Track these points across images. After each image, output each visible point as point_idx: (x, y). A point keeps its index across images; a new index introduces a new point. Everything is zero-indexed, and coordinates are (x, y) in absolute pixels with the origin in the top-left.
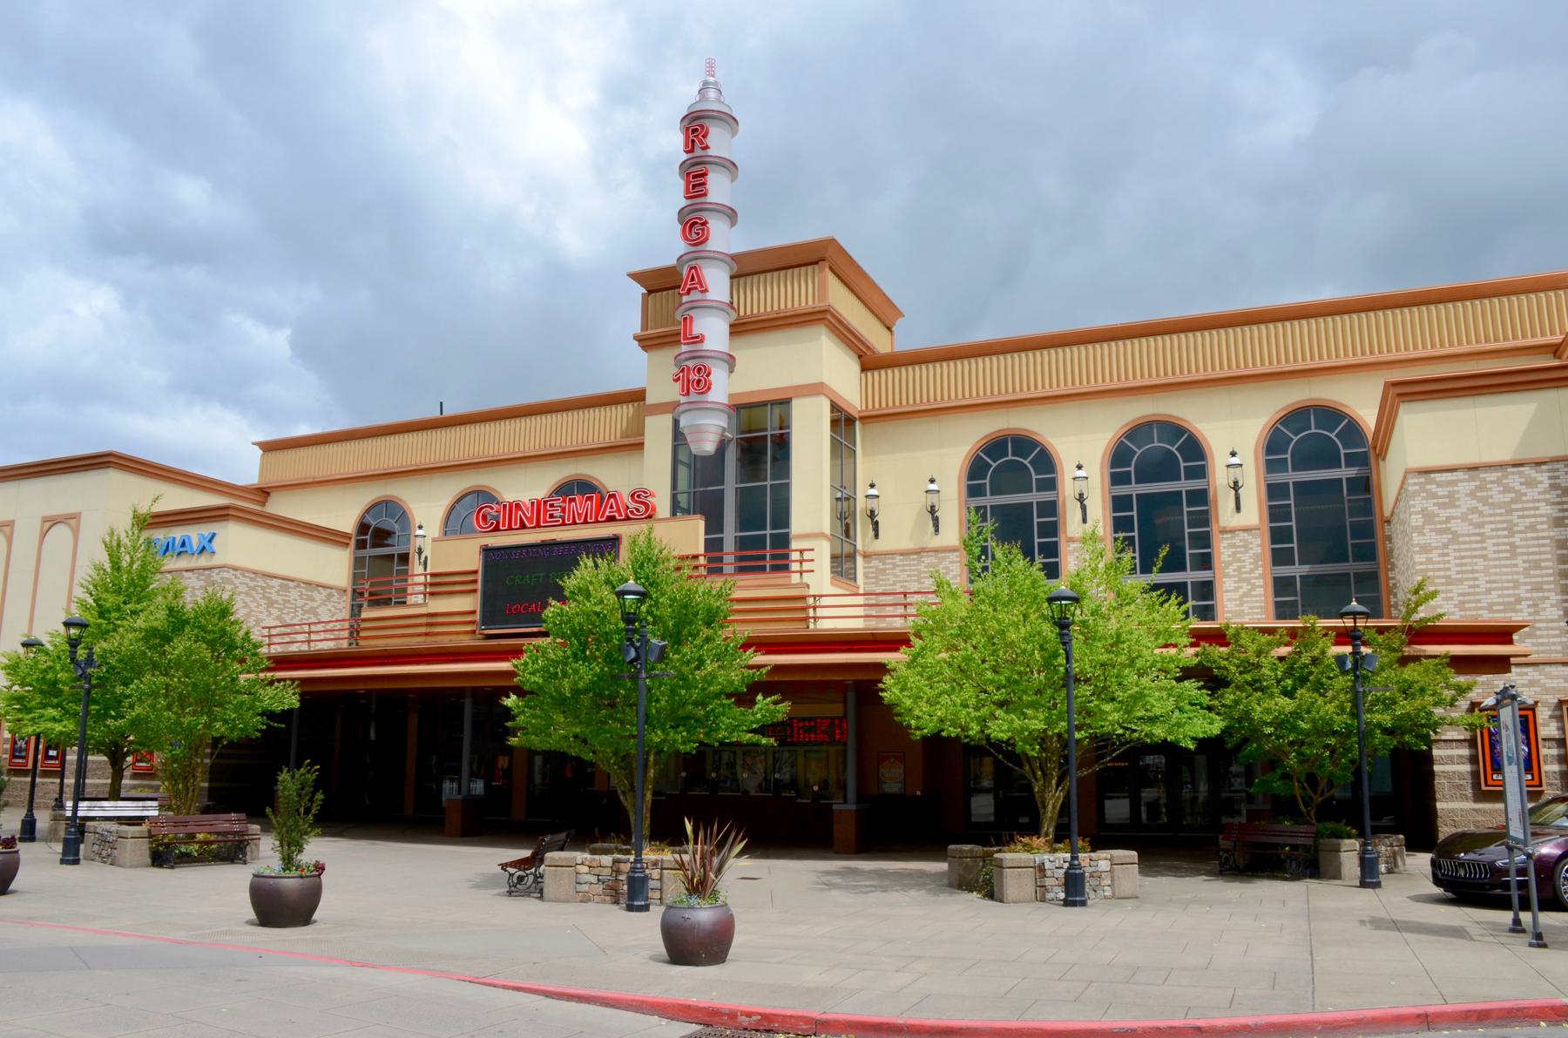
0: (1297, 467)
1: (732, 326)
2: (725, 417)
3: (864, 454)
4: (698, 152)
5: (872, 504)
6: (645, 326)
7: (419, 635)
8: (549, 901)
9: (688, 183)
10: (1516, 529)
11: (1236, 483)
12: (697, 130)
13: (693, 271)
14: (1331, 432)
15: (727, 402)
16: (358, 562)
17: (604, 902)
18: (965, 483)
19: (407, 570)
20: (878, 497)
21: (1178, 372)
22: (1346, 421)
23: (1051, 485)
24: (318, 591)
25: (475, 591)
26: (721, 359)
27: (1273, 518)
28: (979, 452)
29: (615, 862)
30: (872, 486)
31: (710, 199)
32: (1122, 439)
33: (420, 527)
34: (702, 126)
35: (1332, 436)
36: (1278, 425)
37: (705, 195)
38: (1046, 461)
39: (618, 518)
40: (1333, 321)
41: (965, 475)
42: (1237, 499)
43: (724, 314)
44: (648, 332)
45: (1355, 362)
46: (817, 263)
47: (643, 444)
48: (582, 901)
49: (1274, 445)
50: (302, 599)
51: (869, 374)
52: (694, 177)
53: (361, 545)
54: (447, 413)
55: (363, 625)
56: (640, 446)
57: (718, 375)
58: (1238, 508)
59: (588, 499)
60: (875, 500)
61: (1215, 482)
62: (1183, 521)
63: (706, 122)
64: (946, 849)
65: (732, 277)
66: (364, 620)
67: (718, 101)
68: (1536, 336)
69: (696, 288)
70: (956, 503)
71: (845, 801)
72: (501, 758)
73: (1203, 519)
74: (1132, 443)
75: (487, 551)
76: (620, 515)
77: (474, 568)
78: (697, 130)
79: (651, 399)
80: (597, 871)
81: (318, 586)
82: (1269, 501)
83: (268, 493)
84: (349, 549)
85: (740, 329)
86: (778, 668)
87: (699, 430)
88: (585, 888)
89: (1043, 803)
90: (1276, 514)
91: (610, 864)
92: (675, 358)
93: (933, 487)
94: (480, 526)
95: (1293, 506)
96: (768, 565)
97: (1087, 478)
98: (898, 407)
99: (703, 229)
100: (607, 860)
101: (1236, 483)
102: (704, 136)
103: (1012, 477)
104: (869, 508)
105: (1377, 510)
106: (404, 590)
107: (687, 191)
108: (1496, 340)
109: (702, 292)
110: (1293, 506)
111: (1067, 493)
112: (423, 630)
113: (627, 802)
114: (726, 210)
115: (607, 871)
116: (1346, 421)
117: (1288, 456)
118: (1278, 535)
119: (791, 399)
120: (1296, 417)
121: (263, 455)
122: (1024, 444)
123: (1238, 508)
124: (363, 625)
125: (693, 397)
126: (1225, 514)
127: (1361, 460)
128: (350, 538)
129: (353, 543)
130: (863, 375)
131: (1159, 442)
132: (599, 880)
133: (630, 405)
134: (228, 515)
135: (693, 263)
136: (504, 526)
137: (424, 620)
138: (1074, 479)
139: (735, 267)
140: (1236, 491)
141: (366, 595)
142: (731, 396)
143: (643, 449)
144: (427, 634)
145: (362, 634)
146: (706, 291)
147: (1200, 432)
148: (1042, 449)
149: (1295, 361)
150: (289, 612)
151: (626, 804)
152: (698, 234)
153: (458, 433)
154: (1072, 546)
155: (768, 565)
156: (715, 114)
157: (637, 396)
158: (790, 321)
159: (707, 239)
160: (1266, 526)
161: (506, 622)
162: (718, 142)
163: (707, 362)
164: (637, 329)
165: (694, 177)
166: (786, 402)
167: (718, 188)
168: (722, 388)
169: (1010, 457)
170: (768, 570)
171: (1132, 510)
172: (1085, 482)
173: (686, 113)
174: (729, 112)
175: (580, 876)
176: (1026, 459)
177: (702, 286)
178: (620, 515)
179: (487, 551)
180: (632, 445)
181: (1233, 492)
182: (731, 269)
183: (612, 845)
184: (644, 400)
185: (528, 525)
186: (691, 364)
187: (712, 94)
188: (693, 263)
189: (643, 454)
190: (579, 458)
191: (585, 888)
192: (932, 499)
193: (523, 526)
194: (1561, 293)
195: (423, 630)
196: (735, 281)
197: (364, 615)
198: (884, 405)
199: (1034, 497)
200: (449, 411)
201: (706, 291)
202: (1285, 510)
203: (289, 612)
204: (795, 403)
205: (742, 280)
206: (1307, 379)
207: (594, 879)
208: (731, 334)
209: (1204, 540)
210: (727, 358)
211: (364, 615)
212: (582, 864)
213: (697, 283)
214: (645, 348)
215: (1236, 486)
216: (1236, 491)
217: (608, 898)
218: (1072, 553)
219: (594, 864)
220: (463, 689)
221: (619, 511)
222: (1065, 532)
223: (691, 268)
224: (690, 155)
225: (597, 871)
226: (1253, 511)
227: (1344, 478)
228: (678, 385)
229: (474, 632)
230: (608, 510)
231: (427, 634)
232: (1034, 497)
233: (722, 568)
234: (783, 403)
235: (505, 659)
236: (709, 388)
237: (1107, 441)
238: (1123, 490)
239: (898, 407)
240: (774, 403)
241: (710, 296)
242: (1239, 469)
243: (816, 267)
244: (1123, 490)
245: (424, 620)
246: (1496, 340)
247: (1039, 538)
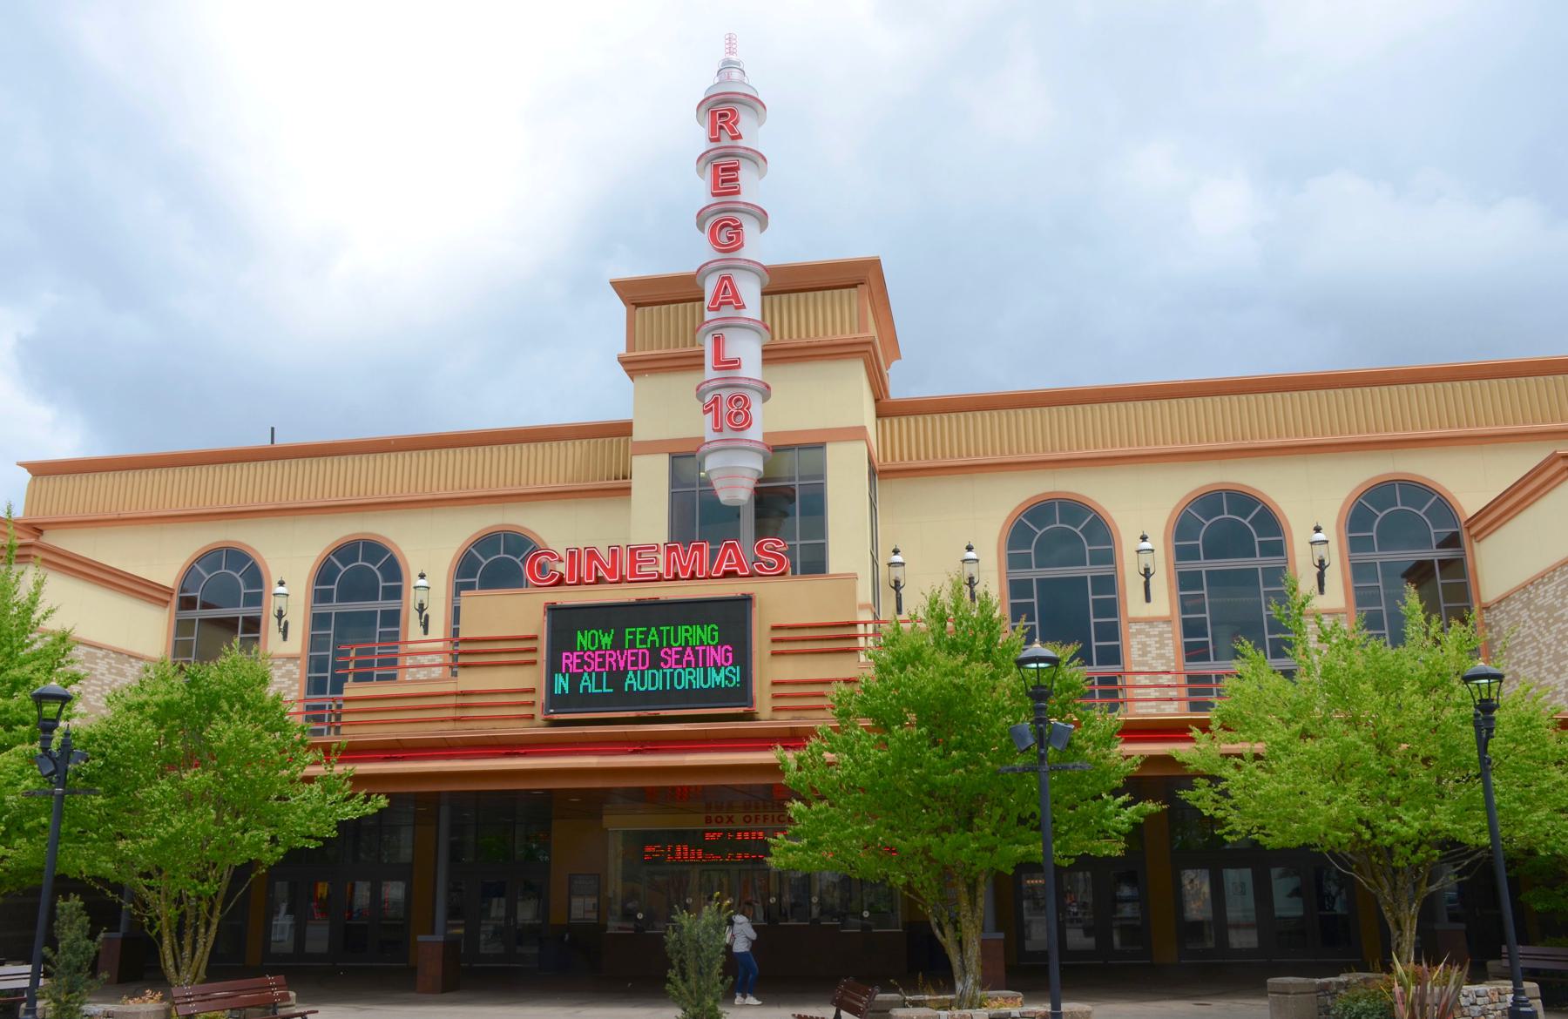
0: (343, 598)
4: (726, 141)
6: (631, 344)
9: (716, 176)
12: (726, 115)
13: (726, 281)
16: (182, 627)
19: (397, 633)
20: (903, 564)
21: (922, 457)
22: (1260, 507)
24: (130, 663)
25: (534, 663)
26: (757, 390)
27: (1184, 610)
28: (1021, 517)
31: (741, 198)
32: (1187, 508)
33: (281, 584)
34: (733, 111)
35: (1246, 522)
36: (1021, 517)
37: (738, 193)
38: (393, 569)
44: (637, 353)
46: (855, 286)
47: (630, 489)
49: (1183, 528)
50: (110, 673)
51: (887, 421)
53: (187, 603)
54: (279, 442)
55: (346, 706)
56: (627, 490)
57: (757, 409)
59: (695, 548)
64: (1265, 985)
65: (764, 294)
66: (347, 700)
68: (1090, 449)
69: (731, 303)
70: (444, 601)
72: (320, 884)
74: (1035, 526)
75: (553, 610)
76: (743, 569)
77: (531, 633)
78: (726, 115)
79: (639, 434)
81: (130, 656)
82: (1356, 582)
83: (41, 531)
84: (168, 609)
85: (772, 356)
86: (1151, 760)
89: (1398, 923)
90: (1186, 605)
92: (698, 389)
93: (971, 555)
94: (534, 578)
95: (1206, 596)
97: (1153, 550)
99: (738, 234)
103: (1227, 541)
104: (893, 578)
105: (1474, 595)
107: (715, 186)
108: (1061, 449)
109: (737, 308)
110: (1206, 596)
112: (451, 713)
113: (948, 940)
116: (1260, 507)
117: (1374, 534)
119: (825, 443)
120: (1208, 502)
121: (33, 481)
122: (374, 549)
124: (346, 706)
126: (1133, 604)
127: (1453, 541)
128: (172, 594)
129: (175, 601)
131: (1229, 513)
134: (28, 556)
135: (725, 273)
136: (701, 573)
139: (767, 279)
140: (897, 591)
143: (630, 494)
144: (455, 720)
145: (345, 718)
146: (743, 307)
150: (95, 691)
151: (943, 940)
153: (124, 479)
154: (1134, 628)
156: (742, 97)
159: (742, 245)
162: (753, 134)
163: (748, 393)
164: (622, 349)
165: (724, 170)
166: (821, 446)
167: (751, 187)
168: (765, 420)
170: (376, 665)
171: (1033, 597)
172: (1325, 546)
173: (703, 98)
174: (756, 96)
176: (1077, 527)
177: (738, 301)
178: (743, 569)
179: (553, 610)
180: (618, 489)
181: (1144, 579)
188: (725, 273)
192: (970, 569)
193: (599, 580)
195: (451, 713)
196: (767, 298)
197: (347, 693)
199: (1088, 571)
200: (281, 441)
201: (743, 307)
202: (326, 639)
203: (95, 691)
204: (830, 448)
209: (1111, 632)
211: (347, 693)
213: (728, 296)
214: (632, 373)
215: (1147, 574)
220: (439, 793)
221: (740, 564)
224: (714, 145)
226: (1164, 602)
227: (1204, 570)
230: (725, 564)
231: (455, 720)
234: (814, 446)
236: (749, 425)
237: (455, 551)
241: (745, 313)
243: (853, 290)
246: (1061, 449)
247: (1095, 617)
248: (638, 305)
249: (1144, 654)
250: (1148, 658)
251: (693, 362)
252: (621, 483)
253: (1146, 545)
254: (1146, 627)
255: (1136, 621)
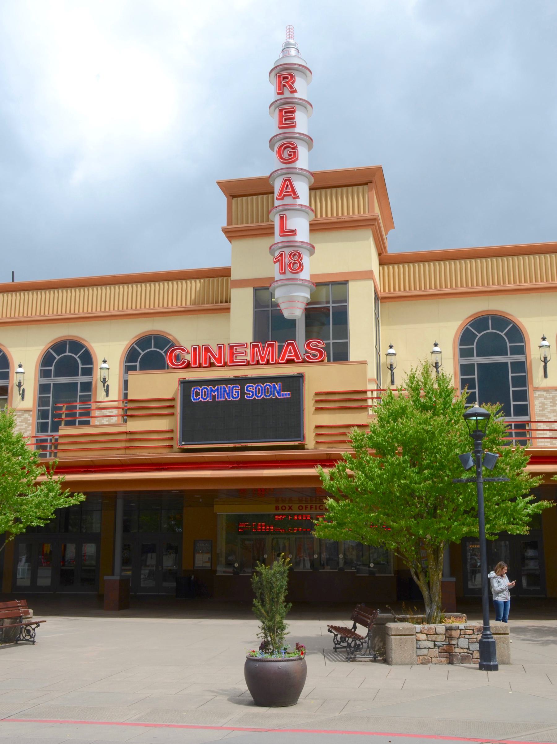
1: (311, 225)
2: (308, 291)
3: (381, 325)
4: (287, 94)
5: (392, 359)
6: (229, 222)
7: (118, 449)
8: (396, 664)
10: (551, 400)
11: (545, 358)
14: (502, 332)
15: (308, 279)
17: (441, 663)
18: (39, 368)
19: (90, 396)
23: (521, 350)
28: (468, 326)
29: (449, 629)
30: (391, 347)
33: (20, 366)
34: (292, 76)
38: (88, 358)
39: (296, 360)
40: (486, 261)
41: (39, 364)
42: (392, 376)
43: (305, 214)
44: (234, 226)
45: (537, 286)
46: (366, 184)
48: (422, 663)
52: (286, 113)
58: (546, 376)
60: (393, 357)
61: (531, 357)
62: (49, 401)
63: (295, 73)
65: (311, 189)
67: (297, 56)
69: (290, 195)
71: (113, 574)
73: (522, 381)
79: (235, 276)
80: (434, 638)
87: (291, 300)
88: (425, 652)
90: (42, 402)
91: (444, 632)
92: (270, 248)
93: (437, 349)
96: (78, 412)
98: (103, 312)
100: (441, 628)
101: (545, 358)
102: (293, 83)
104: (389, 363)
106: (88, 414)
107: (281, 123)
111: (532, 357)
112: (123, 445)
113: (421, 583)
114: (307, 138)
115: (441, 638)
116: (511, 325)
118: (43, 414)
123: (546, 376)
125: (289, 275)
130: (381, 268)
132: (435, 645)
133: (198, 281)
137: (123, 437)
138: (540, 347)
139: (313, 180)
140: (392, 371)
141: (63, 416)
142: (312, 276)
143: (230, 312)
144: (126, 448)
145: (60, 448)
146: (298, 197)
147: (521, 323)
148: (513, 325)
149: (440, 288)
151: (418, 582)
152: (290, 155)
154: (537, 393)
155: (78, 412)
157: (225, 273)
158: (258, 232)
160: (37, 408)
161: (204, 439)
164: (225, 225)
165: (286, 113)
166: (345, 283)
169: (153, 349)
173: (273, 67)
175: (420, 643)
178: (298, 358)
181: (390, 371)
182: (310, 182)
183: (408, 616)
184: (230, 276)
185: (261, 362)
186: (287, 251)
187: (293, 52)
188: (287, 176)
189: (229, 318)
190: (155, 318)
191: (425, 652)
193: (211, 365)
194: (553, 255)
195: (123, 445)
196: (313, 192)
198: (98, 310)
199: (509, 359)
205: (318, 192)
206: (487, 297)
207: (431, 644)
208: (311, 231)
209: (522, 396)
210: (309, 247)
211: (61, 432)
212: (421, 632)
216: (392, 371)
217: (443, 660)
218: (537, 398)
219: (432, 632)
220: (116, 492)
222: (532, 383)
223: (286, 180)
224: (280, 97)
225: (434, 638)
228: (278, 265)
229: (171, 447)
230: (287, 355)
231: (126, 448)
232: (509, 359)
233: (90, 412)
235: (312, 466)
238: (468, 361)
239: (103, 312)
240: (334, 283)
241: (299, 202)
242: (22, 375)
243: (365, 187)
244: (468, 361)
245: (123, 437)
248: (234, 197)
249: (543, 410)
250: (545, 412)
251: (268, 231)
252: (224, 305)
253: (545, 343)
254: (545, 393)
255: (537, 389)
